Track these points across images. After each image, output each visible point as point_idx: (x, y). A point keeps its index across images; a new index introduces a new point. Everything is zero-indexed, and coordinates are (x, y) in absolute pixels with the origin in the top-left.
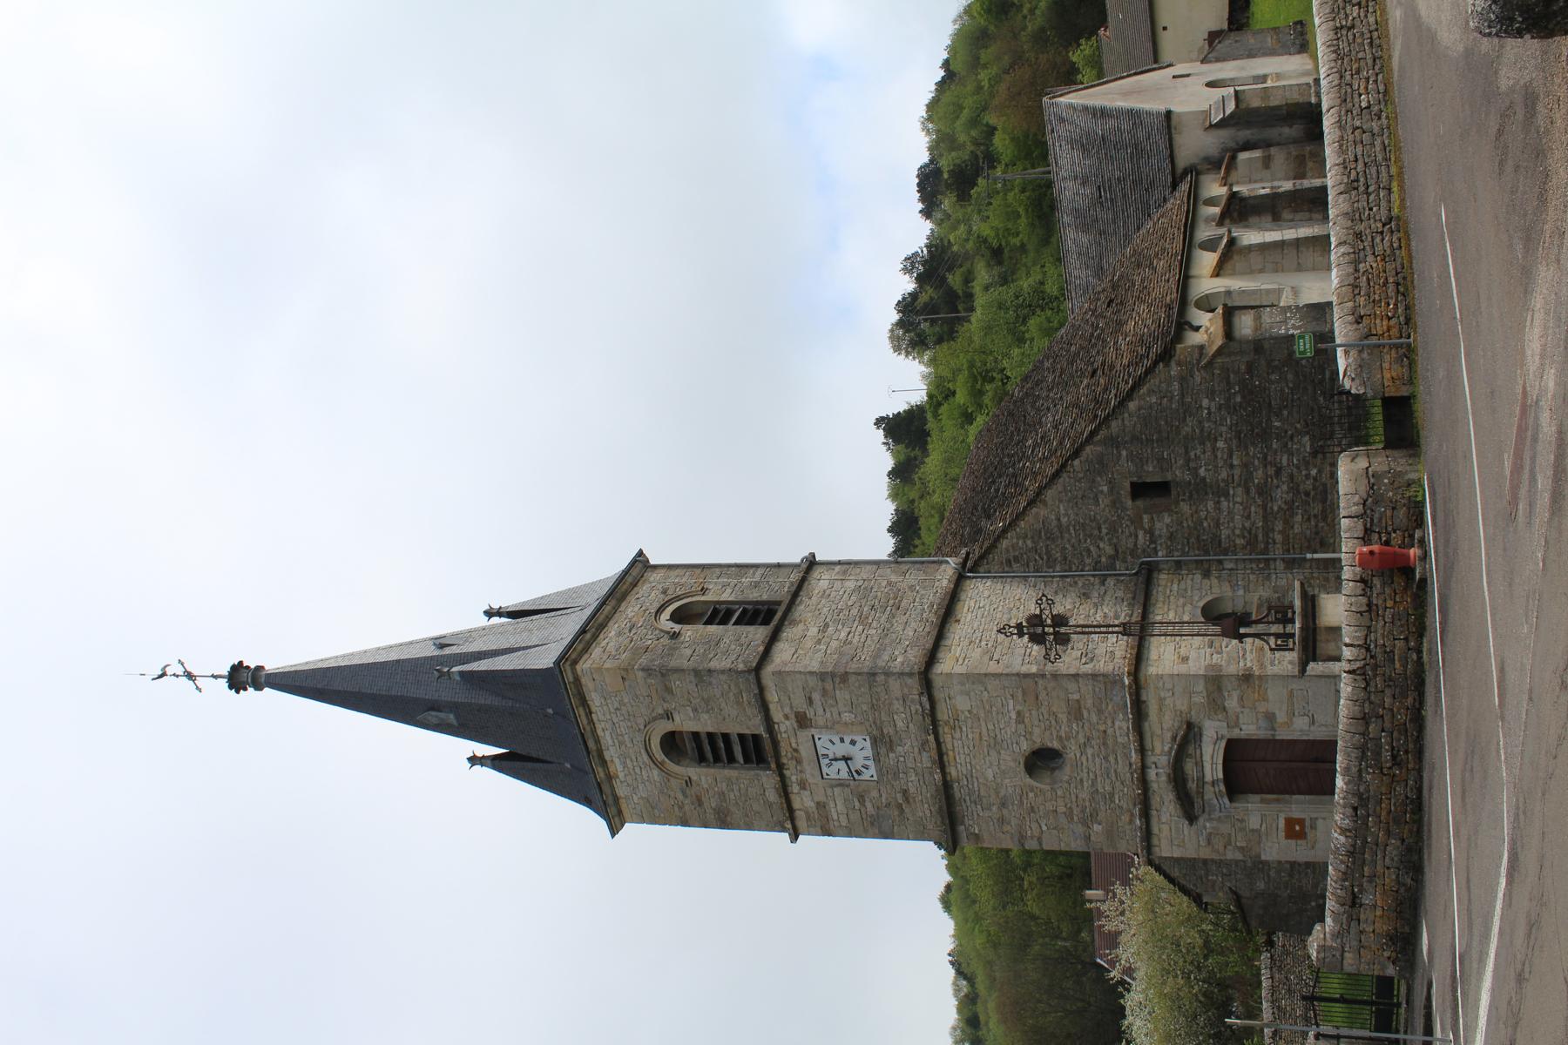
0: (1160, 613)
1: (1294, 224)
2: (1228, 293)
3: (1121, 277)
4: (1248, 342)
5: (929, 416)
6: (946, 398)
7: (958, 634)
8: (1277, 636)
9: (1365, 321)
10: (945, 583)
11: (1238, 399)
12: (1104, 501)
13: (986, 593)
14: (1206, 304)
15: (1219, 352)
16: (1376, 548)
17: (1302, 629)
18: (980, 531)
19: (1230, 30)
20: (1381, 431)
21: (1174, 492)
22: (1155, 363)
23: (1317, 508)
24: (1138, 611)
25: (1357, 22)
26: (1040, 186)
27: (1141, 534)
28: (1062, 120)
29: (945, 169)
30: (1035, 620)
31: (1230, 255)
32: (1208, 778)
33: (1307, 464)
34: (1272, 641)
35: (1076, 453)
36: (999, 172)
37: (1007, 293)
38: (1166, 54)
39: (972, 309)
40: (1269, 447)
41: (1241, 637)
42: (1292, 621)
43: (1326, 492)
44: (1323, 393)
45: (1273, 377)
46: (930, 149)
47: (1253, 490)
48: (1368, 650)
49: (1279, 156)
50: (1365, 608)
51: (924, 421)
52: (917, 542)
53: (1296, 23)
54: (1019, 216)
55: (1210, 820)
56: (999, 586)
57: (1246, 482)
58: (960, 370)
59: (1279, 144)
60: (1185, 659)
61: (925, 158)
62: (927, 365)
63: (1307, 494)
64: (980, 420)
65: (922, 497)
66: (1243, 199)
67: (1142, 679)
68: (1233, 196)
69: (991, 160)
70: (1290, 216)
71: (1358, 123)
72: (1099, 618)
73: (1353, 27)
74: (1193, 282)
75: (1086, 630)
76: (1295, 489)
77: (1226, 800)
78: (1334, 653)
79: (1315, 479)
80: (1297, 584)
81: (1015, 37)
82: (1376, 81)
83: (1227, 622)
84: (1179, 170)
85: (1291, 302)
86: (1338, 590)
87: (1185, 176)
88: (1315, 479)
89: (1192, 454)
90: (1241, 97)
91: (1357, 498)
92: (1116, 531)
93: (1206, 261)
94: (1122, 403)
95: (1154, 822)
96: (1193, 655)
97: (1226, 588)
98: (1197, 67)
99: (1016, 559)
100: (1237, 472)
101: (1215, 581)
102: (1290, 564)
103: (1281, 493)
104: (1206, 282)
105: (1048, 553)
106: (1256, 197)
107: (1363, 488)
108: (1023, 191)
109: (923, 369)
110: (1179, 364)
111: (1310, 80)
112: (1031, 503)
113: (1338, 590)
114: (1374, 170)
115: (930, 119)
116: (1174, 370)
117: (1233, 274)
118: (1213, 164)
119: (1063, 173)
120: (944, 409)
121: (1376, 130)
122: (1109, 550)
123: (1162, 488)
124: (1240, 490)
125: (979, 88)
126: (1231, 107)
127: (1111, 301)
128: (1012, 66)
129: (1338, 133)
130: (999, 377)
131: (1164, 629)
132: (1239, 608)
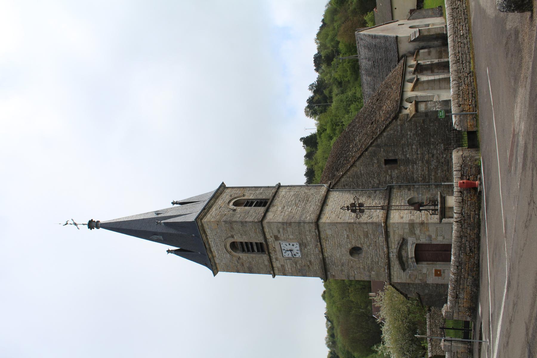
1: (438, 74)
2: (417, 97)
3: (381, 91)
4: (423, 113)
5: (318, 137)
6: (324, 131)
7: (328, 209)
8: (432, 210)
10: (323, 192)
11: (420, 132)
12: (376, 166)
14: (409, 100)
15: (414, 116)
16: (465, 181)
17: (440, 208)
18: (335, 175)
19: (417, 9)
20: (467, 142)
21: (398, 162)
23: (445, 168)
24: (387, 202)
25: (459, 7)
26: (354, 61)
27: (388, 176)
28: (361, 39)
29: (323, 56)
30: (353, 205)
32: (410, 256)
33: (442, 153)
34: (431, 211)
35: (366, 150)
36: (341, 56)
37: (344, 97)
39: (332, 102)
40: (430, 148)
41: (420, 210)
42: (437, 205)
43: (449, 162)
44: (448, 130)
45: (431, 124)
46: (318, 49)
47: (425, 162)
48: (462, 214)
49: (433, 51)
51: (316, 139)
52: (314, 179)
53: (439, 7)
54: (347, 71)
55: (410, 270)
56: (341, 193)
59: (433, 47)
60: (402, 218)
61: (316, 52)
62: (317, 121)
63: (442, 163)
64: (335, 139)
65: (315, 164)
66: (421, 66)
68: (418, 64)
69: (338, 52)
72: (374, 204)
73: (458, 8)
74: (405, 93)
75: (369, 208)
76: (438, 161)
77: (415, 264)
78: (451, 216)
80: (439, 193)
81: (346, 11)
82: (465, 26)
83: (416, 205)
84: (400, 56)
85: (437, 100)
86: (452, 195)
87: (402, 58)
93: (409, 86)
94: (381, 133)
95: (392, 271)
96: (405, 216)
99: (347, 185)
100: (419, 156)
102: (437, 186)
103: (434, 163)
104: (409, 93)
105: (357, 183)
106: (426, 65)
107: (461, 161)
108: (349, 63)
109: (316, 122)
110: (400, 120)
111: (444, 26)
112: (352, 166)
113: (452, 195)
114: (465, 56)
115: (318, 39)
116: (399, 122)
117: (418, 90)
118: (412, 54)
119: (362, 57)
120: (323, 135)
121: (465, 42)
122: (377, 182)
123: (395, 161)
124: (420, 162)
125: (334, 29)
126: (417, 35)
127: (378, 99)
128: (346, 20)
130: (341, 124)
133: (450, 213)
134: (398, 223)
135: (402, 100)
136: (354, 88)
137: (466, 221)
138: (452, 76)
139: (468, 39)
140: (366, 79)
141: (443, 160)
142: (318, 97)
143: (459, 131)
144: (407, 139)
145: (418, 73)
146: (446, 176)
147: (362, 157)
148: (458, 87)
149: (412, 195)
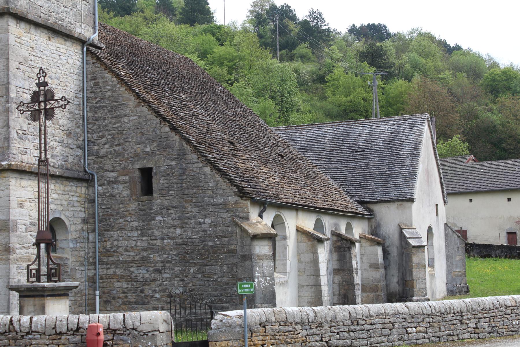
0: (56, 190)
1: (331, 283)
2: (285, 238)
3: (300, 164)
4: (250, 250)
5: (206, 26)
6: (219, 39)
7: (39, 38)
8: (38, 271)
9: (262, 329)
10: (79, 30)
11: (210, 244)
12: (139, 148)
13: (71, 61)
14: (277, 222)
15: (246, 231)
16: (102, 337)
17: (44, 287)
18: (118, 57)
19: (466, 244)
20: (185, 340)
21: (145, 198)
22: (237, 186)
23: (132, 298)
24: (57, 172)
25: (465, 326)
26: (367, 111)
27: (115, 174)
28: (412, 126)
29: (383, 44)
30: (49, 96)
31: (314, 239)
33: (163, 291)
34: (34, 267)
35: (174, 129)
36: (379, 82)
37: (292, 85)
38: (453, 201)
39: (282, 60)
40: (176, 265)
41: (37, 244)
42: (49, 280)
43: (143, 303)
44: (212, 302)
45: (225, 268)
46: (398, 35)
47: (145, 254)
48: (28, 333)
49: (378, 274)
50: (58, 331)
51: (201, 23)
52: (112, 14)
53: (468, 288)
54: (347, 96)
56: (76, 71)
57: (152, 249)
58: (238, 50)
59: (386, 275)
60: (21, 206)
61: (392, 30)
62: (242, 26)
63: (142, 291)
64: (201, 64)
65: (145, 18)
66: (349, 249)
67: (5, 175)
68: (352, 243)
69: (387, 77)
70: (336, 281)
71: (396, 326)
72: (52, 143)
73: (462, 323)
74: (294, 213)
75: (43, 132)
76: (146, 282)
78: (25, 310)
79: (152, 297)
80: (76, 283)
81: (473, 97)
82: (424, 338)
83: (49, 235)
84: (372, 206)
85: (277, 281)
86: (72, 312)
87: (367, 211)
88: (152, 297)
89: (172, 211)
90: (420, 250)
91: (137, 324)
92: (117, 157)
93: (308, 222)
94: (209, 162)
96: (25, 211)
97: (75, 235)
98: (443, 220)
99: (96, 84)
100: (159, 242)
101: (80, 227)
102: (92, 280)
103: (143, 273)
104: (294, 222)
105: (101, 107)
106: (350, 258)
107: (145, 328)
108: (364, 99)
109: (239, 25)
110: (236, 202)
111: (429, 296)
112: (138, 96)
113: (72, 312)
114: (365, 336)
115: (420, 35)
116: (232, 199)
117: (298, 242)
118: (375, 231)
119: (374, 126)
120: (210, 37)
121: (391, 337)
122: (103, 152)
123: (148, 190)
124: (145, 244)
125: (439, 71)
126: (414, 243)
127: (282, 157)
128: (455, 96)
129: (391, 312)
130: (232, 77)
131: (43, 154)
132: (59, 244)
133: (31, 308)
134: (9, 196)
135: (280, 206)
136: (309, 108)
137: (12, 342)
138: (325, 310)
139: (397, 343)
140: (326, 133)
141: (148, 292)
142: (294, 29)
143: (209, 325)
144: (195, 217)
145: (335, 243)
146: (114, 298)
147: (158, 120)
148: (302, 323)
149: (73, 228)
